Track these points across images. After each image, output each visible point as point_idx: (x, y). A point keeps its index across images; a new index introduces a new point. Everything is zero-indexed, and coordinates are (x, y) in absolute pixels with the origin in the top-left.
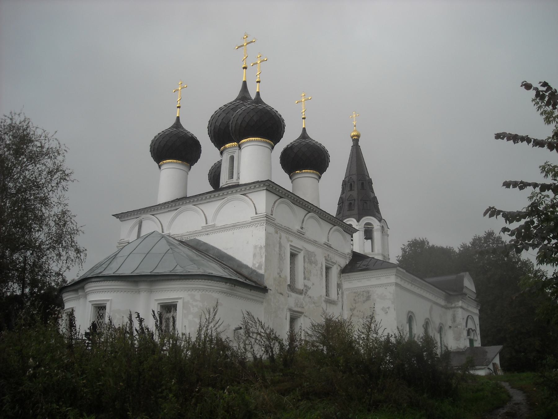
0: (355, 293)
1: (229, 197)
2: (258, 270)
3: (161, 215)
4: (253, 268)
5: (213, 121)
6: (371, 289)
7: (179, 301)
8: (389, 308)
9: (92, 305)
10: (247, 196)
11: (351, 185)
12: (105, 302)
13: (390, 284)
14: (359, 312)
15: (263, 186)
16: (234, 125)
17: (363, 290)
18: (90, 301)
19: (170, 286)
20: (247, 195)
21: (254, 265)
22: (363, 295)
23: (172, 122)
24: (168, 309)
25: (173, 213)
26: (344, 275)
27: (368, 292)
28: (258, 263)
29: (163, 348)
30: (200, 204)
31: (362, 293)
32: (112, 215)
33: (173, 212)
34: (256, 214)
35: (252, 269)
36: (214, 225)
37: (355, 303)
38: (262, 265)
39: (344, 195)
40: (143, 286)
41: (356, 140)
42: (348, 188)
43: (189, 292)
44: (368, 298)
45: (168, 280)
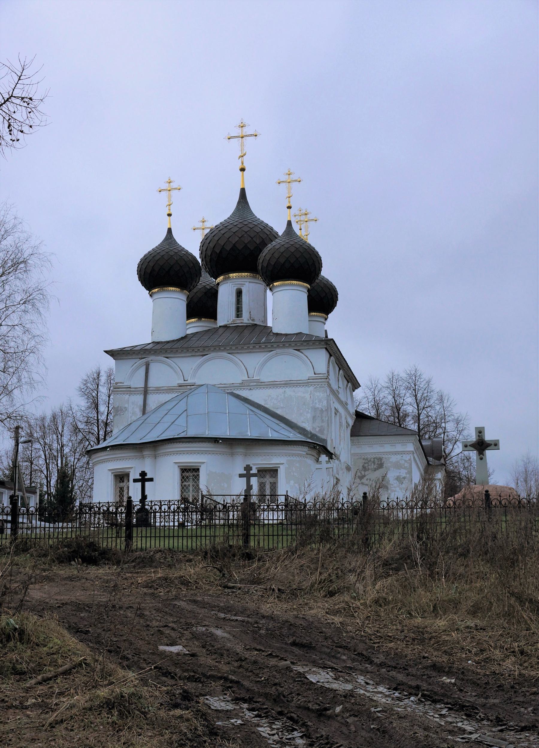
0: (364, 459)
1: (278, 351)
2: (319, 435)
3: (176, 359)
4: (313, 432)
5: (210, 244)
6: (383, 456)
7: (281, 466)
8: (404, 478)
9: (112, 473)
10: (302, 353)
12: (128, 470)
13: (408, 452)
14: (368, 480)
15: (323, 345)
16: (265, 265)
17: (375, 456)
18: (176, 463)
19: (265, 451)
20: (301, 351)
21: (313, 428)
22: (374, 462)
23: (163, 235)
24: (121, 479)
25: (199, 360)
26: (352, 438)
27: (380, 459)
28: (318, 427)
29: (134, 528)
30: (238, 353)
31: (372, 460)
32: (106, 352)
33: (198, 358)
34: (315, 374)
35: (311, 432)
36: (258, 381)
37: (365, 471)
38: (324, 430)
40: (240, 450)
43: (289, 458)
44: (381, 466)
45: (272, 444)
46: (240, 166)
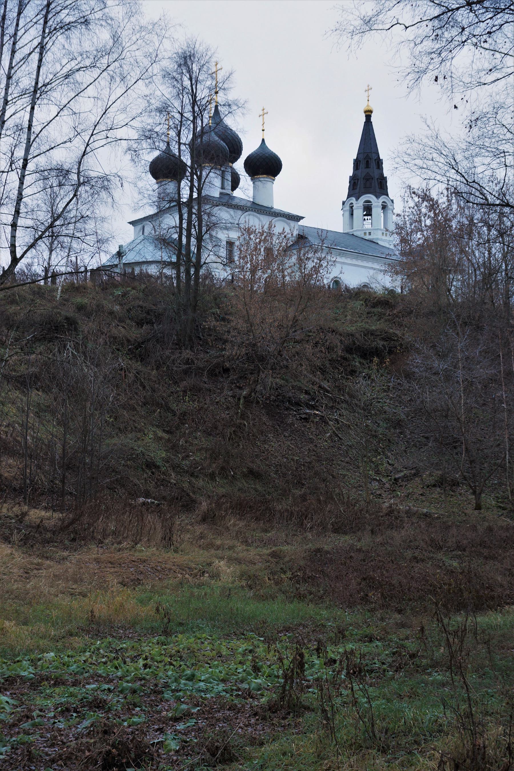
11: (367, 162)
39: (360, 171)
41: (368, 114)
42: (362, 165)
46: (262, 128)
